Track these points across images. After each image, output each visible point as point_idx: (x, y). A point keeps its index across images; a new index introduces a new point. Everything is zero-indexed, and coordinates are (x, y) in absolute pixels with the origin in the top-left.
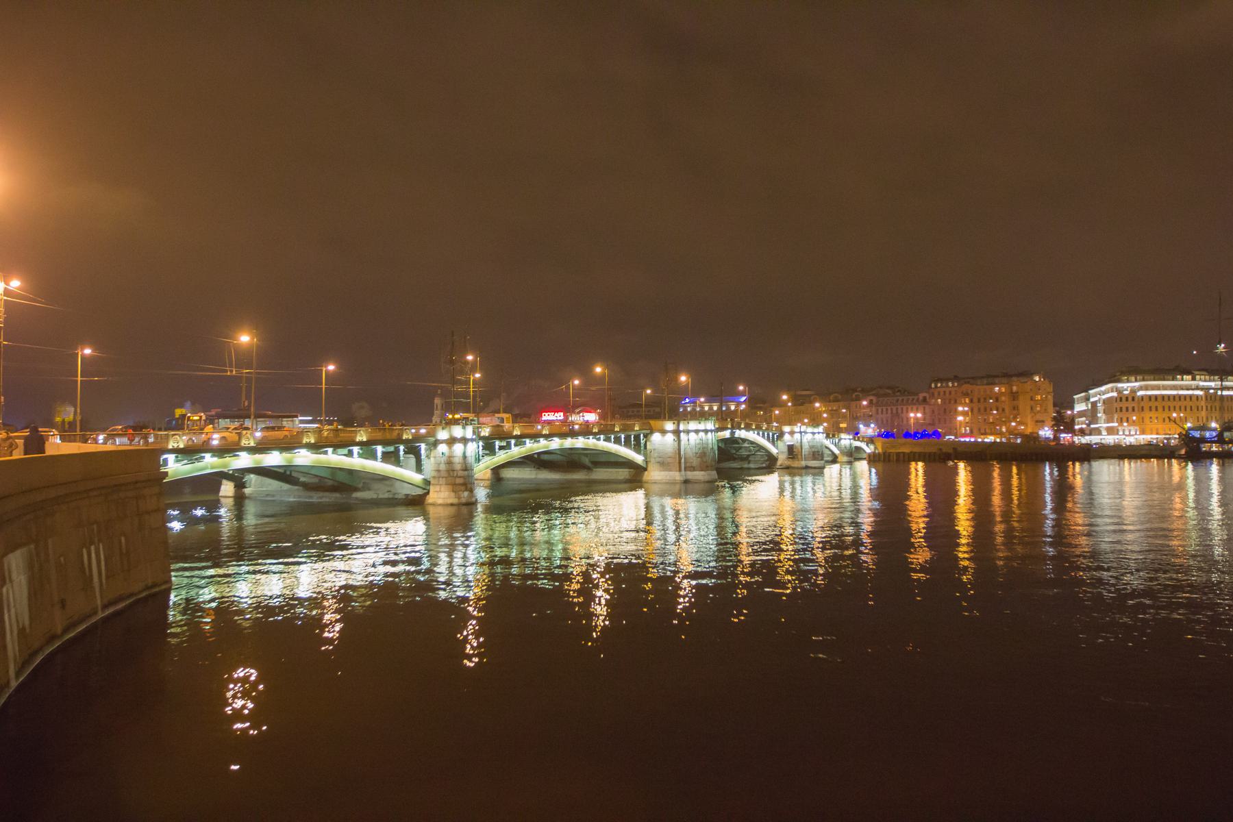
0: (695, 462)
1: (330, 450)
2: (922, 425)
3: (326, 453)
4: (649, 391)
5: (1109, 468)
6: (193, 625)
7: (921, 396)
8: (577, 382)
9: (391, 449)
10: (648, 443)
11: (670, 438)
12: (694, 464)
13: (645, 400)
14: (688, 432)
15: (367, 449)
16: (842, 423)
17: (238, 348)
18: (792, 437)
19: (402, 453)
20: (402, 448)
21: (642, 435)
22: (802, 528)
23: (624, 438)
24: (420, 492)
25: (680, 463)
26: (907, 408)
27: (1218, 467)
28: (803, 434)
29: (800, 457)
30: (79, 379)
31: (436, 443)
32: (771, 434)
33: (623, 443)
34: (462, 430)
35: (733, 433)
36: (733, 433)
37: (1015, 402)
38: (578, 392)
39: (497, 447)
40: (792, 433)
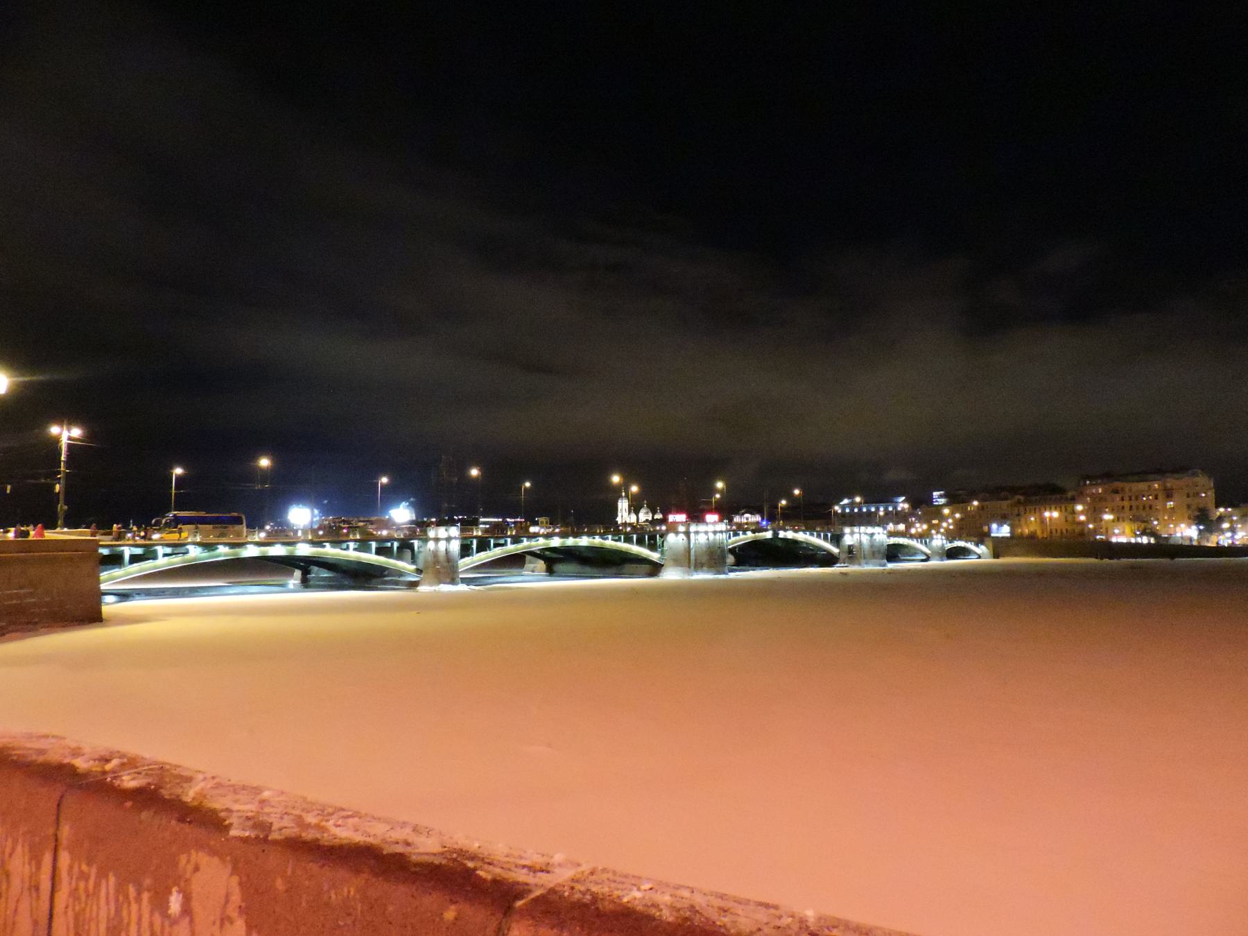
0: (704, 559)
1: (327, 544)
2: (1115, 526)
4: (528, 484)
6: (1061, 507)
7: (1070, 494)
8: (528, 484)
10: (665, 543)
11: (682, 536)
12: (703, 561)
14: (697, 533)
15: (602, 536)
16: (1109, 520)
17: (262, 470)
18: (852, 537)
21: (658, 536)
22: (407, 907)
23: (398, 548)
25: (689, 560)
26: (1035, 509)
28: (863, 535)
29: (858, 556)
30: (173, 491)
31: (426, 540)
35: (776, 534)
36: (776, 534)
37: (450, 563)
39: (127, 558)
40: (852, 533)
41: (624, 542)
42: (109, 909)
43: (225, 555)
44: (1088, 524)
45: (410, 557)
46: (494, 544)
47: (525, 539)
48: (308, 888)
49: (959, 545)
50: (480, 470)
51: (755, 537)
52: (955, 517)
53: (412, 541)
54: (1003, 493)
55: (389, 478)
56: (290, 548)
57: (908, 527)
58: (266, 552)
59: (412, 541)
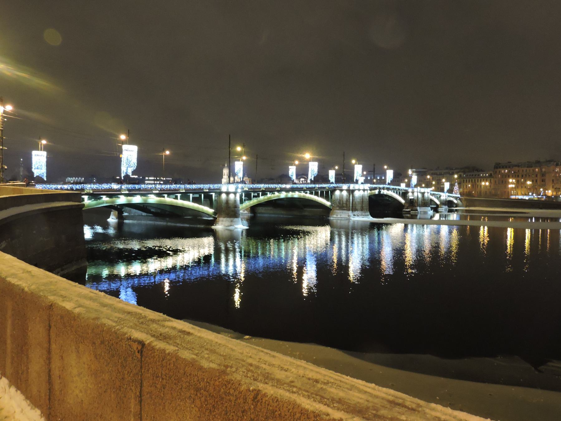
3: (164, 197)
9: (197, 196)
41: (315, 195)
42: (279, 383)
43: (107, 203)
44: (241, 152)
46: (253, 196)
47: (268, 193)
49: (371, 384)
50: (384, 166)
51: (371, 193)
52: (456, 178)
53: (211, 194)
55: (171, 153)
56: (144, 198)
57: (380, 192)
58: (130, 201)
59: (211, 194)
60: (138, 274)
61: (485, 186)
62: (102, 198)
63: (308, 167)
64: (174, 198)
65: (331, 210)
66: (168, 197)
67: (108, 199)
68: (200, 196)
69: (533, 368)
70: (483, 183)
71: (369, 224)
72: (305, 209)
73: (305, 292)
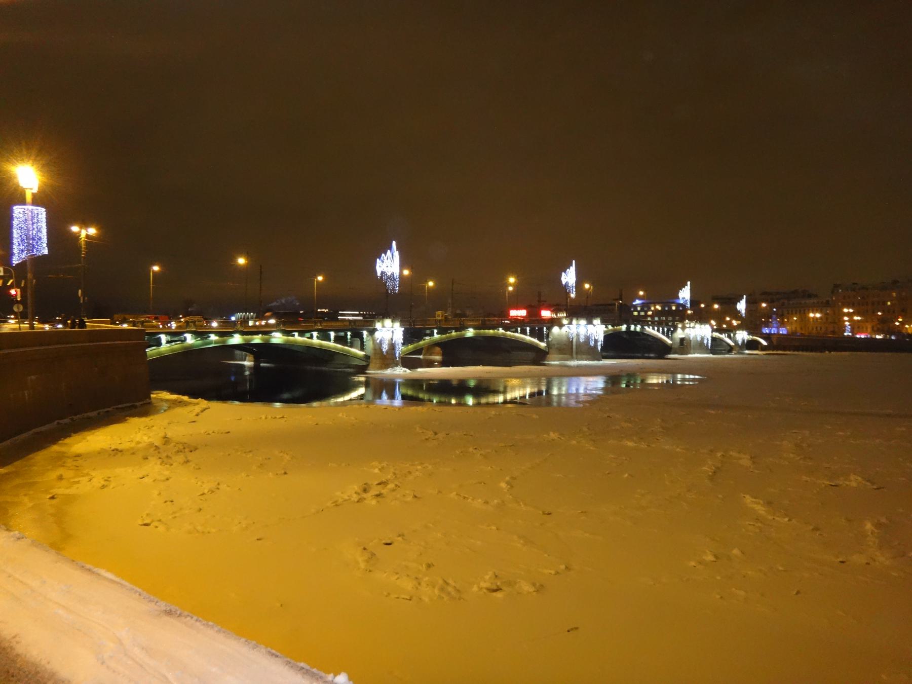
3: (293, 336)
5: (577, 390)
9: (342, 334)
13: (316, 294)
19: (349, 337)
20: (349, 333)
24: (364, 363)
27: (104, 570)
30: (151, 285)
32: (666, 329)
33: (528, 334)
34: (391, 323)
38: (736, 319)
45: (359, 346)
48: (395, 474)
54: (876, 291)
60: (508, 400)
61: (814, 318)
62: (209, 337)
63: (25, 194)
64: (308, 338)
65: (547, 353)
66: (299, 335)
67: (217, 338)
68: (346, 335)
69: (832, 353)
70: (811, 315)
71: (402, 401)
72: (514, 352)
73: (583, 441)
